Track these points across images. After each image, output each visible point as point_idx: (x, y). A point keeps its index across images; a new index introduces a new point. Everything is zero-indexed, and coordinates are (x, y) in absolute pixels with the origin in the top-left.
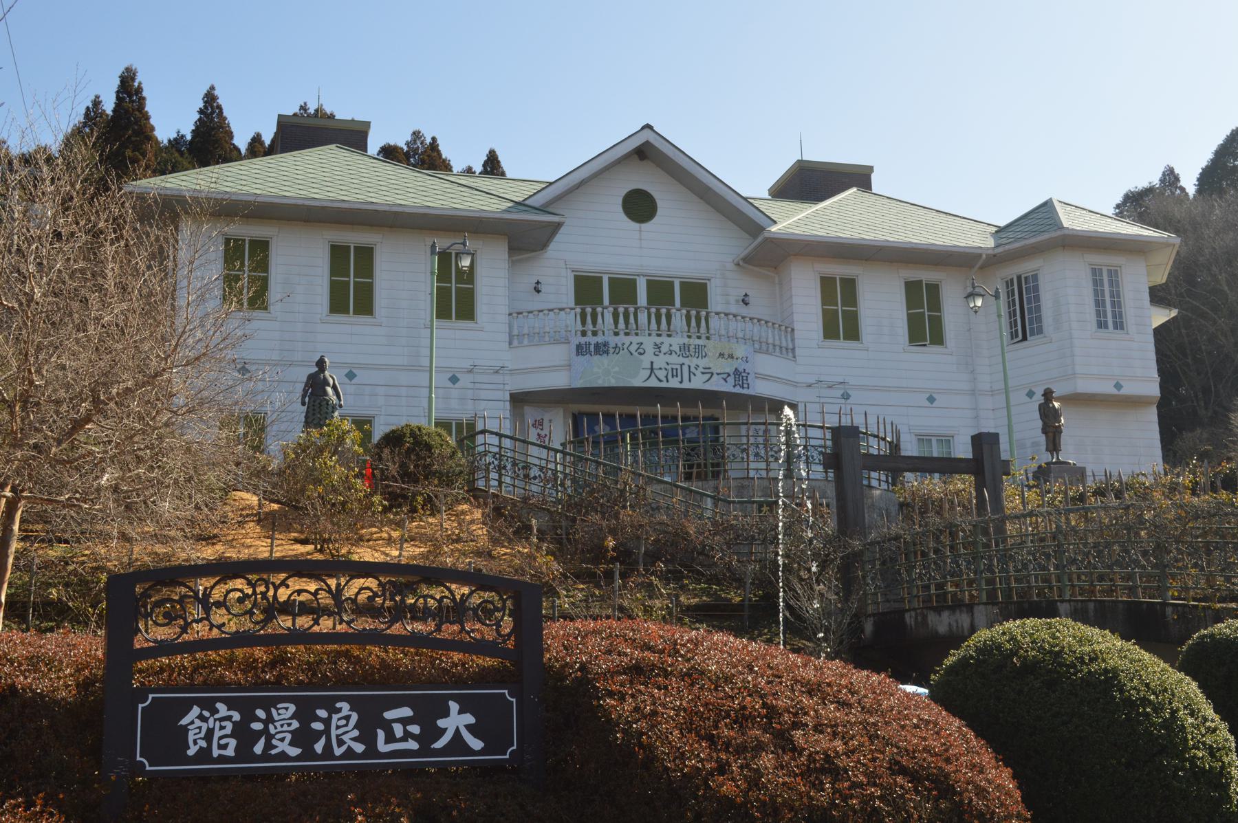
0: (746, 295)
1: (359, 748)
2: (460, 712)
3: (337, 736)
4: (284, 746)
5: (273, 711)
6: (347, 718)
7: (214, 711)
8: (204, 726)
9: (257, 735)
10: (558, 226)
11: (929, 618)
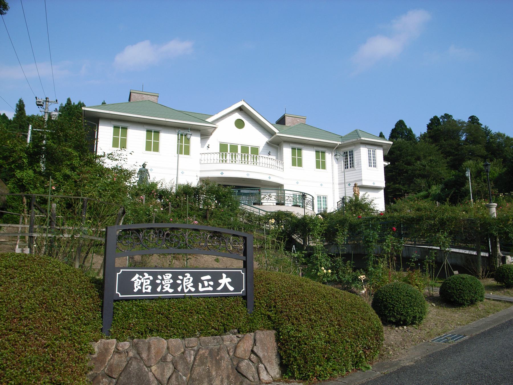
1: (193, 289)
6: (189, 279)
7: (144, 276)
9: (159, 284)
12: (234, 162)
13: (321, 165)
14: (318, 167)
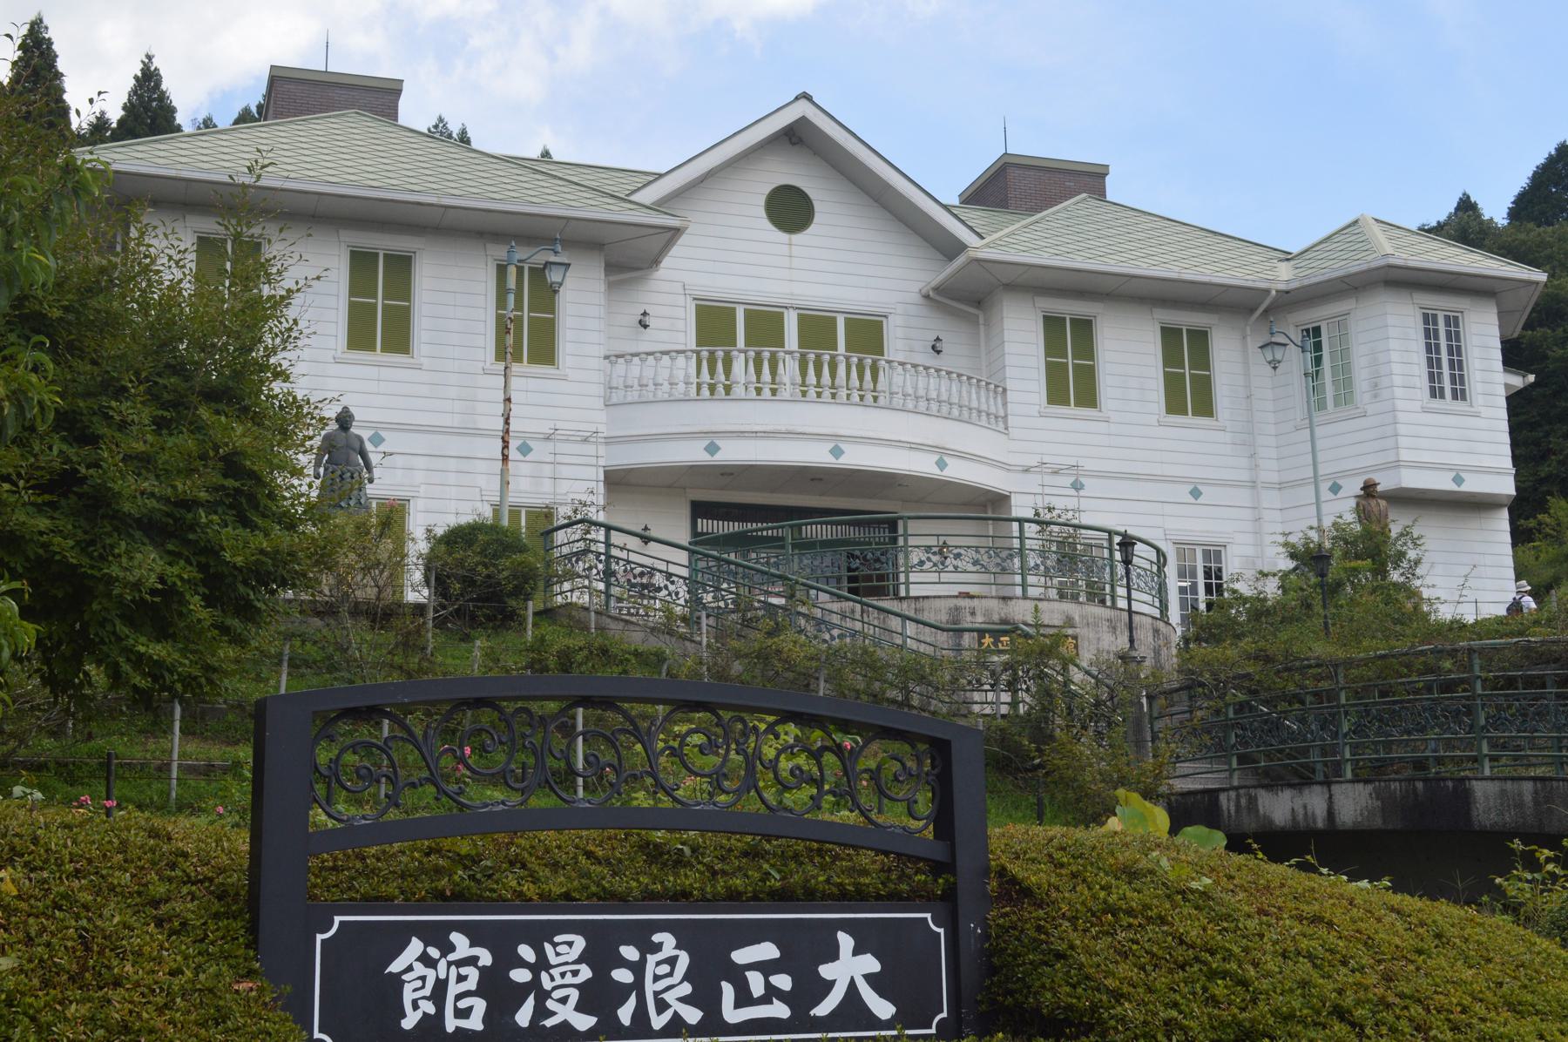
0: (938, 339)
1: (693, 1015)
2: (856, 952)
3: (656, 994)
4: (569, 1014)
5: (548, 947)
6: (672, 962)
7: (448, 948)
8: (431, 975)
9: (522, 991)
10: (676, 232)
11: (1260, 802)
12: (767, 393)
13: (1189, 392)
14: (1175, 404)
